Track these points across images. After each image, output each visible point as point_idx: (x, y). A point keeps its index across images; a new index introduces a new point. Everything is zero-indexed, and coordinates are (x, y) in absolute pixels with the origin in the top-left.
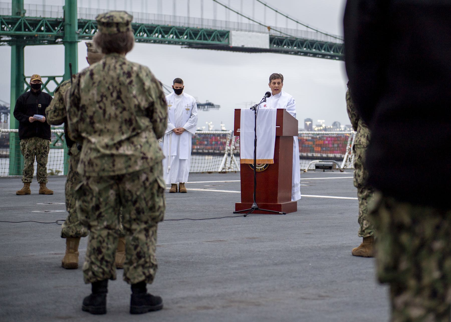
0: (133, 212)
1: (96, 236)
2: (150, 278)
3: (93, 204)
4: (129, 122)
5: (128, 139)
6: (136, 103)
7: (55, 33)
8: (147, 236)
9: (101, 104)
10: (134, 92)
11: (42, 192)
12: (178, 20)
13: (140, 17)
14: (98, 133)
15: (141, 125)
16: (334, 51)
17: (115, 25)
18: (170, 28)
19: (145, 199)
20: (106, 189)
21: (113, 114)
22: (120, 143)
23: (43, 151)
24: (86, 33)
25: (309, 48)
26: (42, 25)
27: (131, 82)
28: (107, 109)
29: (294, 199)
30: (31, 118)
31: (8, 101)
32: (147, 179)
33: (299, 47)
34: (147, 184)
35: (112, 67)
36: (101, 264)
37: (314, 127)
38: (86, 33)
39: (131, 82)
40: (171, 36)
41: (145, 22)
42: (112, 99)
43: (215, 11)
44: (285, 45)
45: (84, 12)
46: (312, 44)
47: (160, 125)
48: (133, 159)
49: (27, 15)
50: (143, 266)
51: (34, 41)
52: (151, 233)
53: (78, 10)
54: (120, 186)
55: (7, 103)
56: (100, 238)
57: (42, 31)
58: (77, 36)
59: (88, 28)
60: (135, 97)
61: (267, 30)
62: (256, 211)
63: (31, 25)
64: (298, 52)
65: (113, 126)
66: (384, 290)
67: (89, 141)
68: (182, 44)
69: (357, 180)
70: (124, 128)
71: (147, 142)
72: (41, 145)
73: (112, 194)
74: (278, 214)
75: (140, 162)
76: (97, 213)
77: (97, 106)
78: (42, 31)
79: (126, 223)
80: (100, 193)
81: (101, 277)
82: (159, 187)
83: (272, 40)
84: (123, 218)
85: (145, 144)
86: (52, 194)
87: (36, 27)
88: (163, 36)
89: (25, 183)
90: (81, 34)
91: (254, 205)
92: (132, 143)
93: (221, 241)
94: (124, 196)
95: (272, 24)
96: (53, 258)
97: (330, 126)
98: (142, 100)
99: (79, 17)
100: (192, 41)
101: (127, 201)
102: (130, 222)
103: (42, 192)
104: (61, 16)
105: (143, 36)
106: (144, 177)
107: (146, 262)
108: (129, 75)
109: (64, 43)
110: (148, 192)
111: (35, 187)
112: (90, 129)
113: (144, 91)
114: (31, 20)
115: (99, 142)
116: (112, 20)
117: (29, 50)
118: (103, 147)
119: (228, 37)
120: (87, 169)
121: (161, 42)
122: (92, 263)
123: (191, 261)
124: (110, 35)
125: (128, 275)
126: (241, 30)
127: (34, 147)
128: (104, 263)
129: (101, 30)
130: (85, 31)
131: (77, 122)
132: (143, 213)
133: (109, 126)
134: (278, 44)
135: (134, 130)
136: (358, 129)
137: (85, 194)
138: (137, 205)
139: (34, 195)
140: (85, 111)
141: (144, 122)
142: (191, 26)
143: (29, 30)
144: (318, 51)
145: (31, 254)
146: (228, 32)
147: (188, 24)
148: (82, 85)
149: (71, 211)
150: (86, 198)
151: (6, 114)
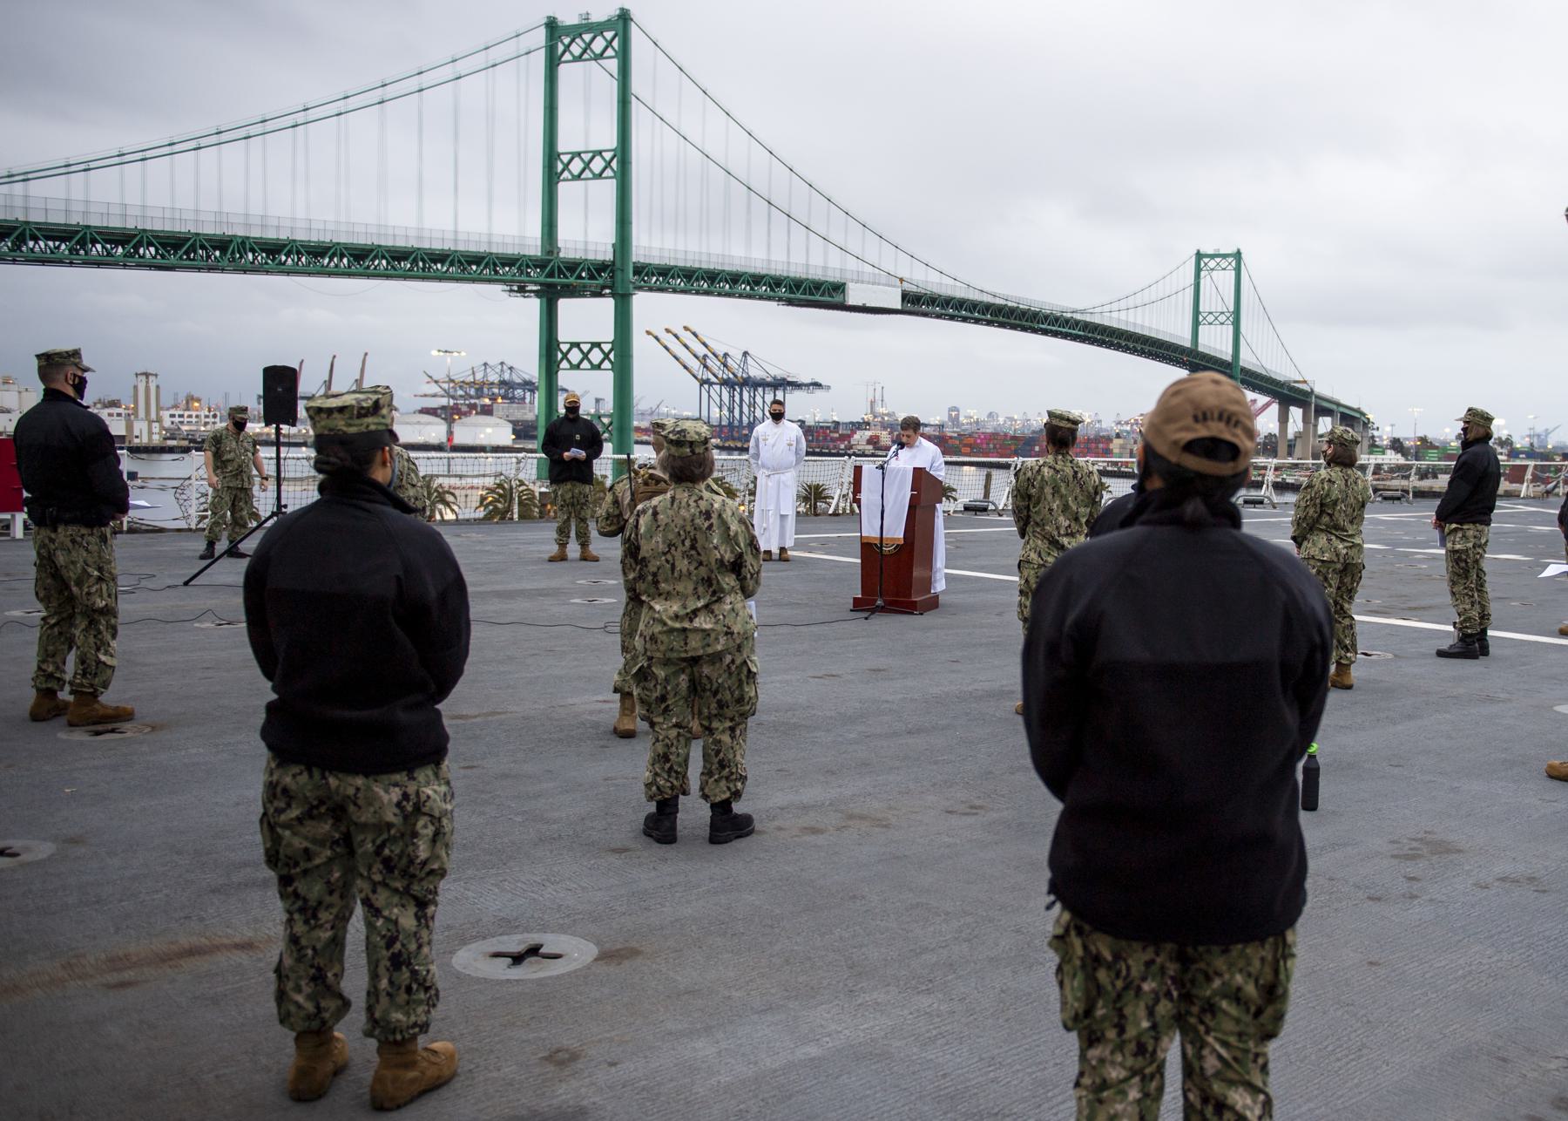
0: (714, 705)
1: (661, 738)
2: (737, 795)
3: (657, 694)
4: (708, 582)
5: (706, 606)
6: (719, 556)
7: (600, 281)
8: (733, 737)
9: (669, 557)
10: (715, 541)
11: (584, 558)
12: (773, 266)
13: (720, 261)
14: (663, 597)
15: (725, 586)
16: (991, 315)
17: (688, 445)
18: (763, 277)
19: (729, 688)
20: (676, 674)
21: (685, 570)
22: (695, 612)
23: (583, 501)
24: (645, 282)
25: (957, 309)
26: (583, 270)
27: (711, 525)
28: (677, 564)
29: (935, 588)
30: (566, 454)
31: (536, 374)
32: (733, 661)
33: (943, 307)
34: (733, 668)
35: (683, 504)
36: (669, 776)
37: (961, 419)
38: (645, 282)
39: (711, 525)
40: (764, 288)
41: (727, 268)
42: (684, 549)
43: (826, 253)
44: (923, 304)
45: (641, 252)
46: (961, 304)
47: (751, 583)
48: (713, 635)
49: (562, 255)
50: (727, 778)
51: (572, 292)
52: (738, 732)
53: (634, 249)
54: (695, 669)
55: (533, 377)
56: (667, 741)
57: (583, 278)
58: (631, 286)
59: (647, 275)
60: (716, 548)
61: (898, 282)
62: (883, 610)
63: (568, 269)
64: (942, 314)
65: (686, 587)
66: (1072, 1040)
67: (651, 608)
68: (779, 301)
69: (1022, 612)
70: (701, 589)
71: (733, 609)
72: (580, 493)
73: (683, 679)
74: (912, 614)
75: (722, 640)
76: (663, 706)
77: (663, 558)
78: (583, 278)
79: (704, 719)
80: (667, 680)
81: (668, 794)
82: (749, 671)
83: (905, 296)
84: (700, 713)
85: (729, 612)
86: (597, 561)
87: (574, 272)
88: (752, 289)
89: (560, 544)
90: (637, 283)
91: (879, 602)
92: (712, 612)
93: (833, 676)
94: (700, 683)
95: (905, 275)
96: (600, 711)
97: (983, 417)
98: (726, 551)
99: (634, 259)
100: (792, 296)
101: (704, 690)
102: (709, 718)
103: (584, 558)
104: (609, 257)
105: (724, 286)
106: (728, 658)
107: (732, 773)
108: (707, 515)
109: (613, 295)
110: (734, 678)
111: (573, 549)
112: (652, 590)
113: (729, 538)
114: (567, 262)
115: (666, 610)
116: (685, 436)
117: (565, 306)
118: (671, 618)
119: (843, 291)
120: (648, 646)
121: (749, 297)
122: (656, 774)
123: (792, 721)
124: (681, 458)
125: (706, 791)
126: (862, 282)
127: (570, 495)
128: (673, 774)
129: (669, 449)
130: (643, 280)
131: (634, 579)
132: (728, 707)
133: (680, 588)
134: (913, 303)
135: (714, 593)
136: (1027, 538)
137: (646, 679)
138: (719, 696)
139: (572, 560)
140: (646, 566)
141: (729, 581)
142: (792, 275)
143: (566, 277)
144: (969, 314)
145: (570, 701)
146: (844, 284)
147: (788, 271)
148: (642, 530)
149: (628, 656)
150: (646, 684)
151: (532, 391)
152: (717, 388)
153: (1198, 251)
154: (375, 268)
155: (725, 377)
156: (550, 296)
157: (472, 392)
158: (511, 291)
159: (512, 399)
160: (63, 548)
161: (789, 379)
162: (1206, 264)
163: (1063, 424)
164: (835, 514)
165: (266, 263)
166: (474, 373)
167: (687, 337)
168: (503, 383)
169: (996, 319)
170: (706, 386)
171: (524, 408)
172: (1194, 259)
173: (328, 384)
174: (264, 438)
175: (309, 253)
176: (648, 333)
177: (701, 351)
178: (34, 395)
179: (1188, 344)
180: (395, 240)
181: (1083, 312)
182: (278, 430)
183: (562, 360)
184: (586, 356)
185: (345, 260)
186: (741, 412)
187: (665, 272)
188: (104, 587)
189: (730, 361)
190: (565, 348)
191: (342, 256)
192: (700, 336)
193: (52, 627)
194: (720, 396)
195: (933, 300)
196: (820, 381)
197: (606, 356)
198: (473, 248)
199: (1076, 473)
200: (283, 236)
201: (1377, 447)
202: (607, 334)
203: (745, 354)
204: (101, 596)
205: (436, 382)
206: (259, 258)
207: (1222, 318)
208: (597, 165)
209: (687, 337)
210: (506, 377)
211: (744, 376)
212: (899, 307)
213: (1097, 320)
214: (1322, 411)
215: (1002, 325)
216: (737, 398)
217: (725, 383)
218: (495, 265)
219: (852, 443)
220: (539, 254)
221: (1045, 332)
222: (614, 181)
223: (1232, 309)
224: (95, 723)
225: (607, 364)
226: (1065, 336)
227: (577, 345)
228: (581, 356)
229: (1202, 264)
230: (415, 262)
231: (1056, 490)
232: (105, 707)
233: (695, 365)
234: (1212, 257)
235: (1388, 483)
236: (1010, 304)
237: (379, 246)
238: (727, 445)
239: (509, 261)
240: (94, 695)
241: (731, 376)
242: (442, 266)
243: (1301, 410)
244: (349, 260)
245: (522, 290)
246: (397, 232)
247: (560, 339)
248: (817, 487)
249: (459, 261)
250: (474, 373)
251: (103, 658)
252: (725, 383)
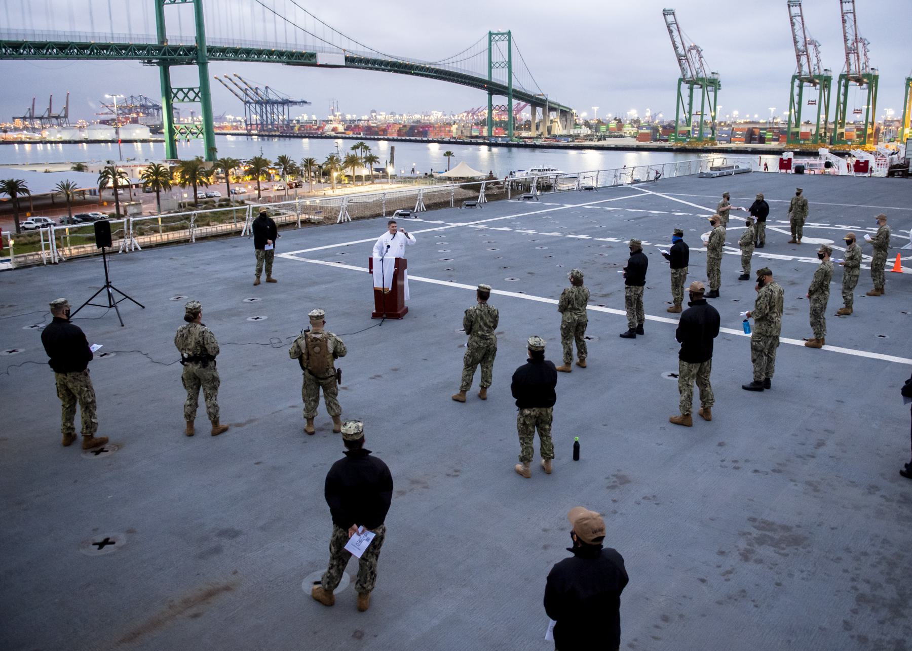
7: (190, 56)
26: (181, 51)
53: (206, 39)
58: (207, 59)
59: (214, 52)
78: (181, 55)
83: (347, 59)
88: (269, 57)
90: (210, 57)
95: (346, 48)
99: (207, 44)
104: (194, 44)
109: (197, 63)
117: (173, 69)
119: (315, 57)
134: (351, 62)
146: (315, 54)
152: (254, 105)
153: (490, 32)
154: (71, 54)
155: (257, 99)
156: (165, 65)
157: (126, 111)
158: (144, 63)
159: (148, 114)
160: (70, 381)
161: (290, 100)
162: (494, 38)
163: (484, 290)
164: (341, 222)
165: (13, 54)
166: (126, 101)
167: (236, 80)
168: (142, 106)
169: (393, 69)
170: (248, 104)
171: (155, 118)
173: (50, 110)
174: (19, 140)
175: (35, 48)
176: (216, 78)
177: (244, 87)
178: (50, 319)
179: (487, 78)
180: (80, 39)
181: (435, 64)
182: (103, 249)
183: (174, 97)
184: (186, 95)
185: (55, 50)
186: (267, 117)
187: (224, 50)
188: (90, 393)
189: (259, 91)
190: (175, 91)
191: (53, 48)
192: (243, 79)
193: (67, 408)
194: (256, 109)
195: (360, 60)
196: (306, 100)
197: (197, 95)
198: (122, 42)
199: (489, 311)
200: (20, 39)
201: (578, 125)
202: (196, 83)
203: (267, 87)
204: (89, 397)
205: (107, 107)
206: (8, 51)
207: (503, 65)
209: (236, 80)
210: (144, 102)
211: (267, 98)
212: (344, 64)
213: (442, 68)
214: (552, 109)
215: (396, 72)
216: (264, 110)
217: (257, 102)
218: (135, 50)
219: (324, 131)
220: (157, 43)
221: (417, 74)
222: (193, 4)
223: (507, 60)
224: (93, 447)
225: (197, 99)
226: (427, 76)
227: (181, 90)
228: (184, 95)
229: (492, 38)
230: (92, 51)
231: (482, 318)
232: (96, 440)
233: (241, 94)
234: (497, 34)
235: (583, 143)
236: (399, 61)
237: (73, 43)
238: (261, 134)
239: (142, 48)
240: (92, 436)
241: (260, 99)
242: (107, 52)
243: (542, 109)
244: (57, 51)
245: (150, 62)
246: (81, 34)
247: (172, 87)
248: (311, 160)
249: (116, 49)
250: (126, 101)
251: (93, 420)
252: (257, 102)
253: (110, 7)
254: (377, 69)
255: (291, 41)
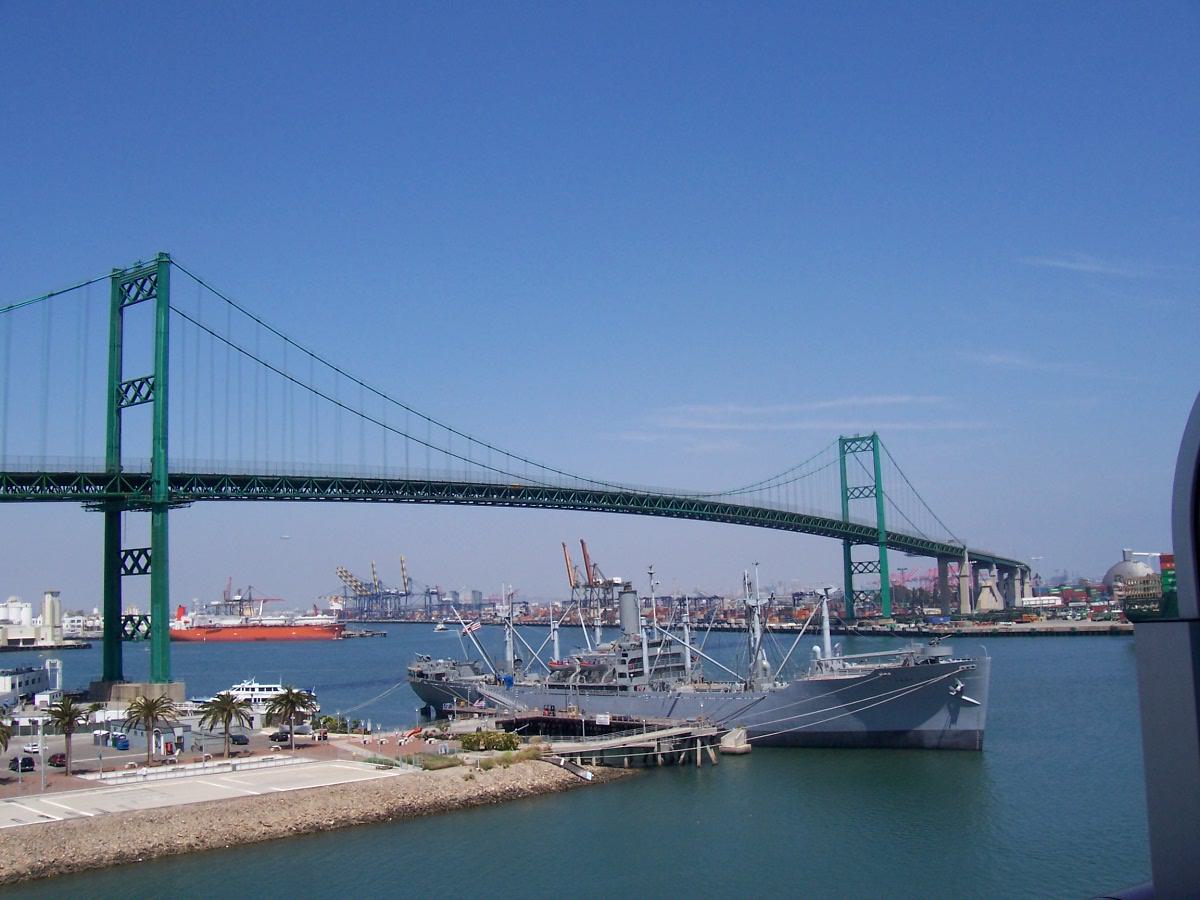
172: (838, 444)
202: (856, 578)
208: (131, 393)
234: (853, 441)
253: (6, 404)
254: (544, 506)
255: (783, 501)
